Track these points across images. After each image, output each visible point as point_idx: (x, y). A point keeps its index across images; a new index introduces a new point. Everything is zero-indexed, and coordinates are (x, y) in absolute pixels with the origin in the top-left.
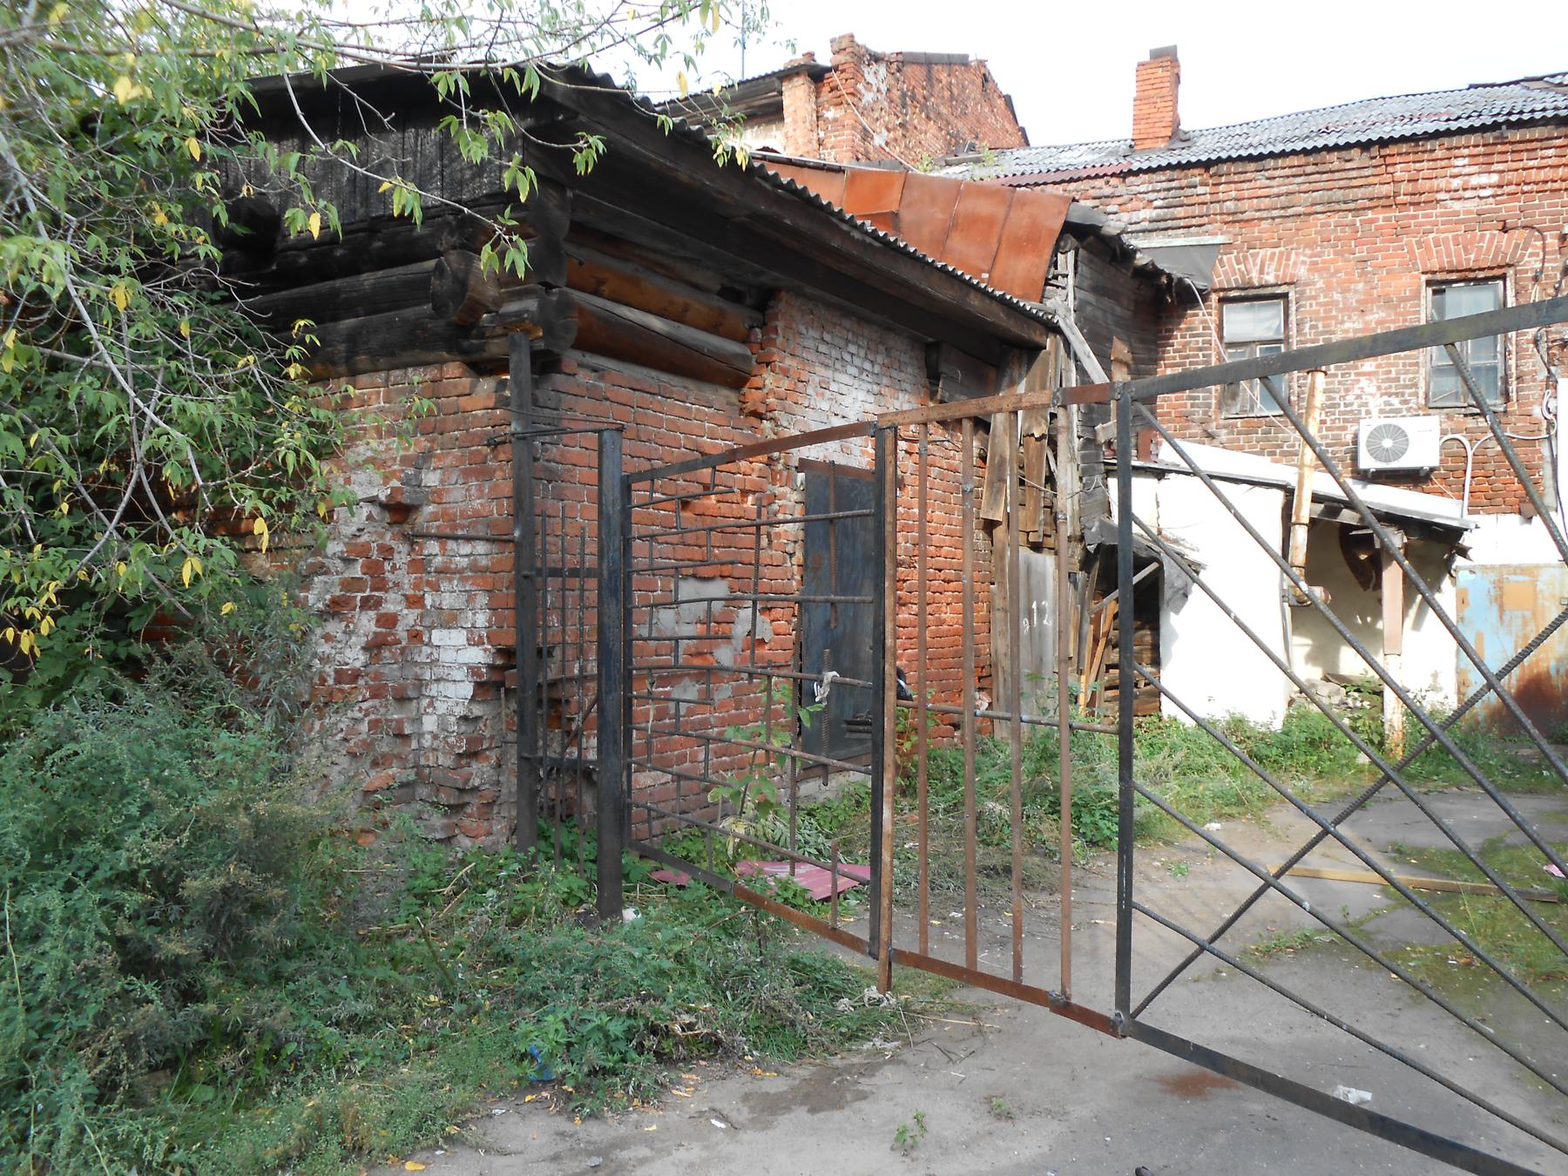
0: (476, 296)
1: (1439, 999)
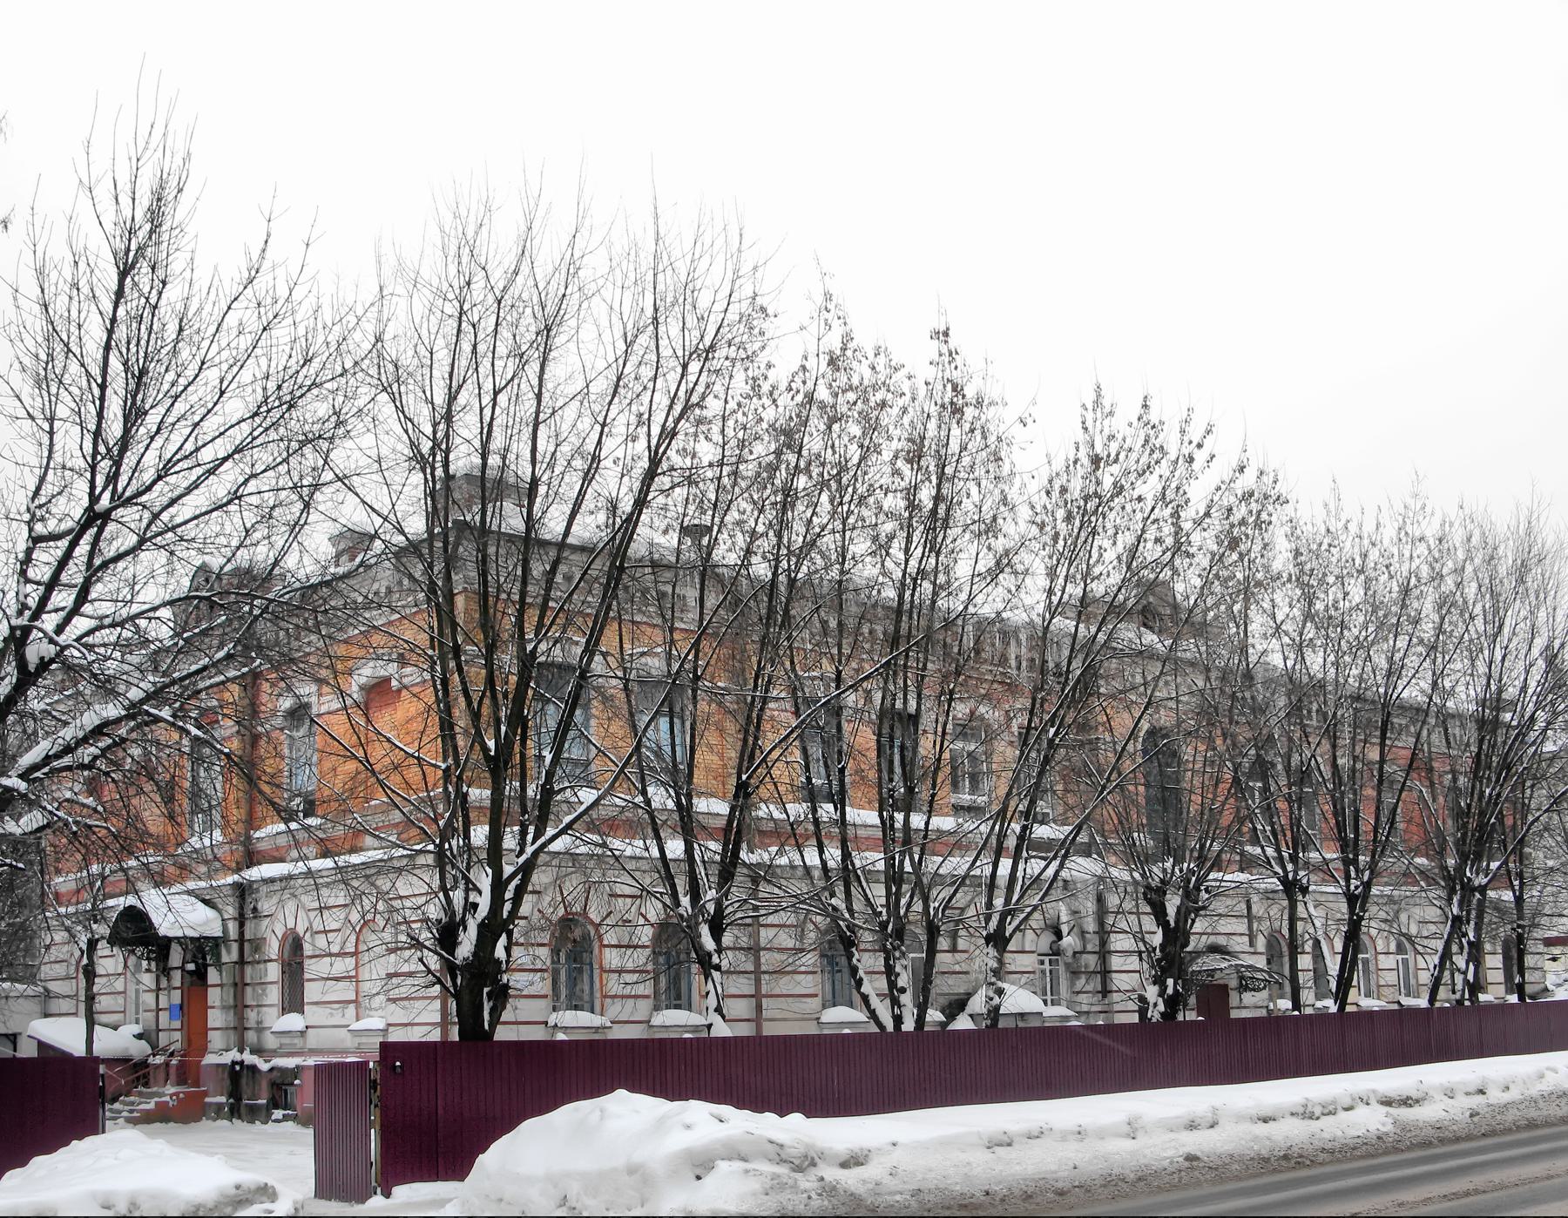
1: (182, 440)
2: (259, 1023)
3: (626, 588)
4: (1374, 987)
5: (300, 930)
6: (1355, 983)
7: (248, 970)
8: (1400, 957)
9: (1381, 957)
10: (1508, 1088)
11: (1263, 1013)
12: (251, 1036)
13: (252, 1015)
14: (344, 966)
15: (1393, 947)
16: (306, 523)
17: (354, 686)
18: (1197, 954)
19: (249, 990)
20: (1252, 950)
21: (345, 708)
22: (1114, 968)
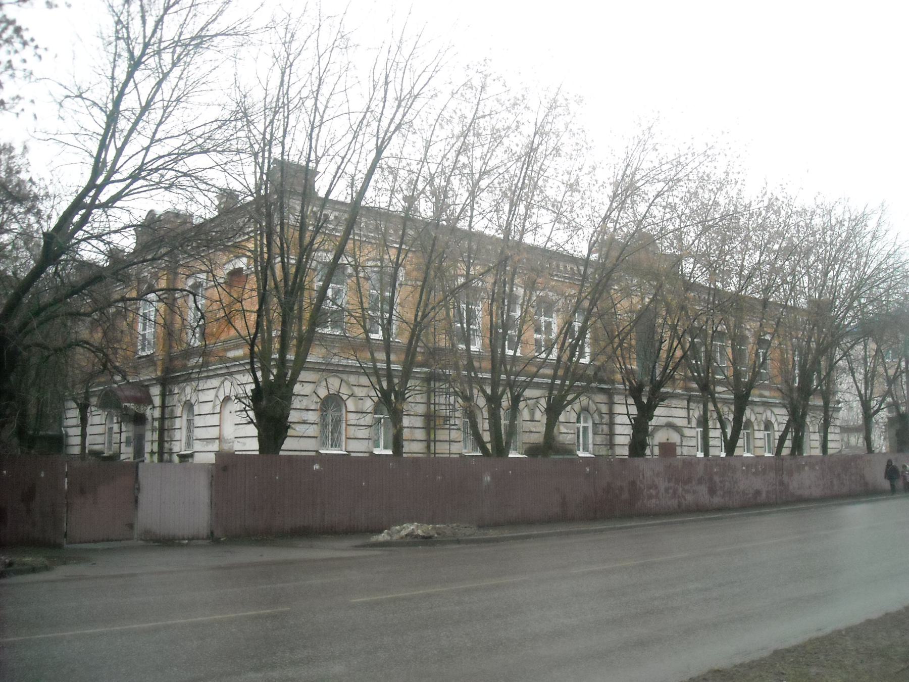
0: (672, 441)
2: (171, 449)
3: (477, 203)
4: (751, 447)
5: (193, 401)
6: (777, 442)
7: (166, 422)
8: (766, 432)
9: (756, 432)
10: (224, 470)
11: (313, 454)
12: (166, 456)
13: (166, 445)
14: (215, 420)
15: (762, 428)
16: (322, 123)
17: (221, 274)
18: (657, 428)
19: (166, 432)
20: (689, 426)
21: (216, 286)
22: (617, 433)
